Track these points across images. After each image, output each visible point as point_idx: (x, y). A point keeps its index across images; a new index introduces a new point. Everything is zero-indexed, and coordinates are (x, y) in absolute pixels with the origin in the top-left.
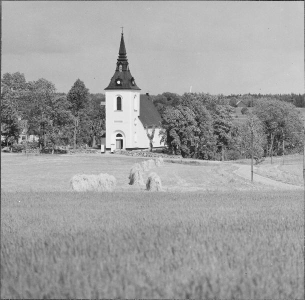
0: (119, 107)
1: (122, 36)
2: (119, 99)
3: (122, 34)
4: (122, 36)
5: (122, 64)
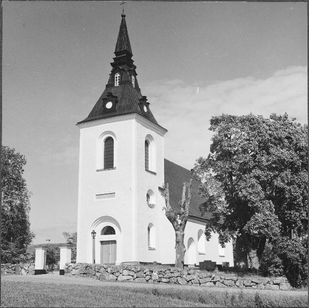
0: (109, 163)
1: (123, 26)
2: (109, 142)
3: (123, 16)
4: (123, 26)
5: (120, 71)
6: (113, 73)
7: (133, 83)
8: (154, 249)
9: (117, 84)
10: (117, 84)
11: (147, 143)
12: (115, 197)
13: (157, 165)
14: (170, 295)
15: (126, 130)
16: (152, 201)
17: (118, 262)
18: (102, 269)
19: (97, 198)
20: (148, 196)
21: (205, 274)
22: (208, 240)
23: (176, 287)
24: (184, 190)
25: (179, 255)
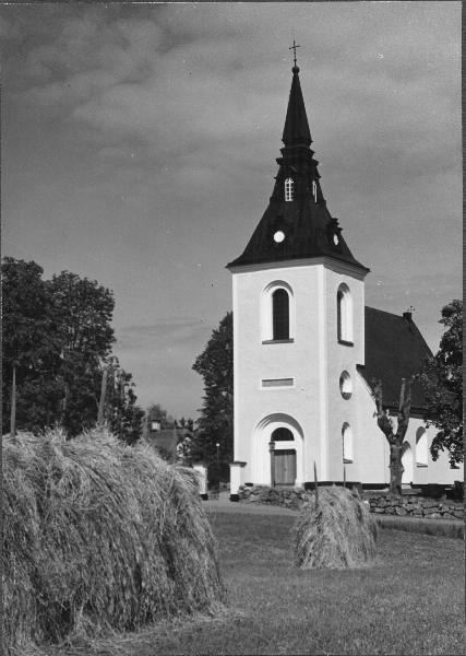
0: (281, 332)
1: (296, 81)
2: (281, 301)
3: (296, 70)
4: (296, 81)
6: (280, 180)
7: (315, 192)
8: (350, 462)
9: (289, 198)
10: (289, 198)
11: (340, 296)
12: (292, 384)
13: (354, 329)
14: (396, 527)
15: (310, 281)
16: (347, 388)
17: (300, 481)
18: (293, 495)
19: (264, 386)
20: (342, 381)
21: (430, 503)
22: (434, 460)
23: (392, 518)
24: (403, 389)
25: (394, 478)
